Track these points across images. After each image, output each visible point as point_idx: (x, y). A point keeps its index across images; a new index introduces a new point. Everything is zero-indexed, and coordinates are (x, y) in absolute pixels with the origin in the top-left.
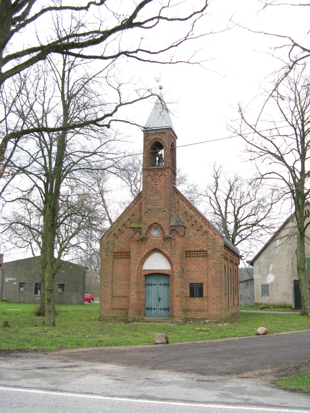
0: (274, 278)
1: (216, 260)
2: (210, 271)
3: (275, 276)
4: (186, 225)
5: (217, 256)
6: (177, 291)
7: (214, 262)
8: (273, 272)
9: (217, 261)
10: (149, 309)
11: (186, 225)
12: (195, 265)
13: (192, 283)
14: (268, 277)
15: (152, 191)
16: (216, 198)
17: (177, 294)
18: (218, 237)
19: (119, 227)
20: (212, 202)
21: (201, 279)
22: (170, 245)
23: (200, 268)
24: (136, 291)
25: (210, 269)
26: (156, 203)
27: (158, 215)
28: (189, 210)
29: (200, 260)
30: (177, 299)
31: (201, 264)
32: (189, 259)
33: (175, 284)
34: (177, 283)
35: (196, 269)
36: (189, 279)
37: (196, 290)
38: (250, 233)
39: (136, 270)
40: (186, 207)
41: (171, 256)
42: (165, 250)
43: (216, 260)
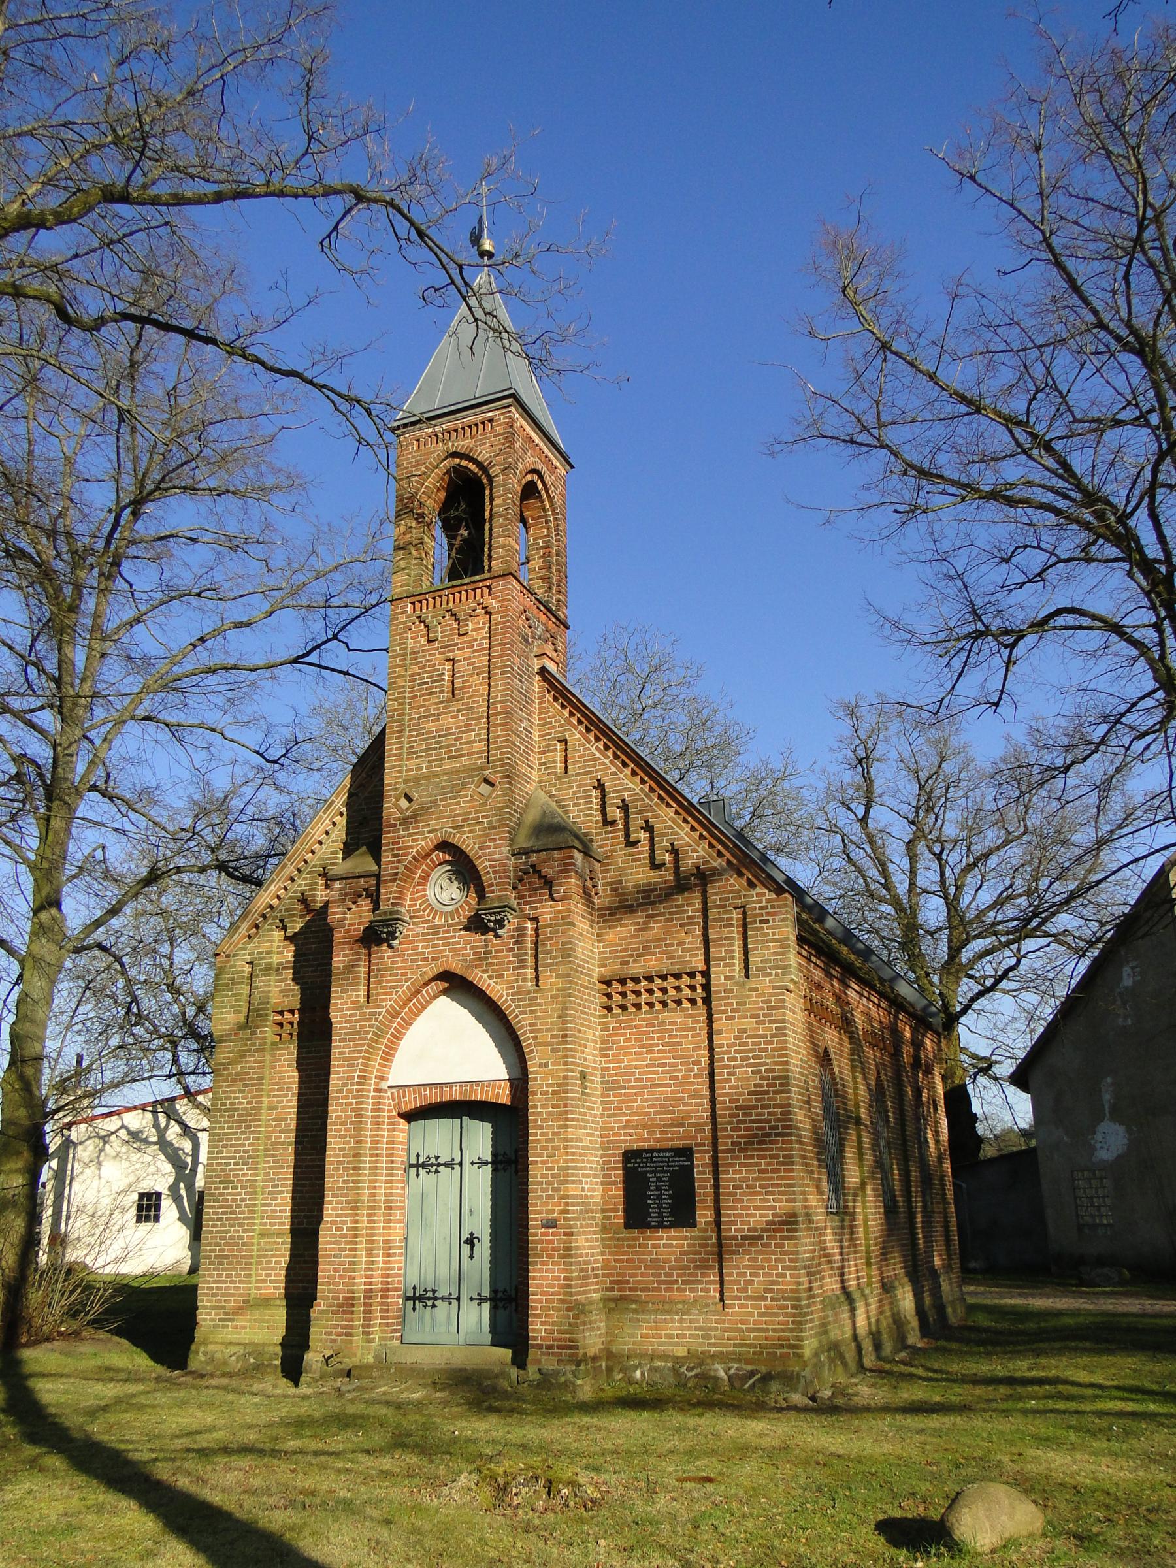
0: (1126, 1141)
1: (758, 1016)
2: (729, 1081)
3: (1129, 1131)
4: (601, 846)
5: (763, 995)
6: (548, 1197)
7: (745, 1030)
8: (1117, 1115)
9: (763, 1022)
10: (421, 1298)
11: (601, 846)
12: (649, 1052)
13: (635, 1146)
14: (1099, 1137)
15: (430, 694)
16: (871, 839)
17: (547, 1212)
18: (763, 895)
19: (299, 885)
20: (857, 854)
21: (682, 1125)
22: (512, 950)
23: (676, 1064)
24: (348, 1202)
25: (728, 1066)
26: (448, 746)
27: (459, 803)
28: (613, 773)
29: (675, 1023)
30: (548, 1242)
31: (679, 1044)
32: (620, 1022)
33: (541, 1155)
34: (546, 1148)
35: (657, 1072)
36: (624, 1128)
37: (658, 1188)
38: (1013, 961)
39: (351, 1091)
40: (599, 759)
41: (517, 1007)
42: (490, 977)
43: (758, 1016)
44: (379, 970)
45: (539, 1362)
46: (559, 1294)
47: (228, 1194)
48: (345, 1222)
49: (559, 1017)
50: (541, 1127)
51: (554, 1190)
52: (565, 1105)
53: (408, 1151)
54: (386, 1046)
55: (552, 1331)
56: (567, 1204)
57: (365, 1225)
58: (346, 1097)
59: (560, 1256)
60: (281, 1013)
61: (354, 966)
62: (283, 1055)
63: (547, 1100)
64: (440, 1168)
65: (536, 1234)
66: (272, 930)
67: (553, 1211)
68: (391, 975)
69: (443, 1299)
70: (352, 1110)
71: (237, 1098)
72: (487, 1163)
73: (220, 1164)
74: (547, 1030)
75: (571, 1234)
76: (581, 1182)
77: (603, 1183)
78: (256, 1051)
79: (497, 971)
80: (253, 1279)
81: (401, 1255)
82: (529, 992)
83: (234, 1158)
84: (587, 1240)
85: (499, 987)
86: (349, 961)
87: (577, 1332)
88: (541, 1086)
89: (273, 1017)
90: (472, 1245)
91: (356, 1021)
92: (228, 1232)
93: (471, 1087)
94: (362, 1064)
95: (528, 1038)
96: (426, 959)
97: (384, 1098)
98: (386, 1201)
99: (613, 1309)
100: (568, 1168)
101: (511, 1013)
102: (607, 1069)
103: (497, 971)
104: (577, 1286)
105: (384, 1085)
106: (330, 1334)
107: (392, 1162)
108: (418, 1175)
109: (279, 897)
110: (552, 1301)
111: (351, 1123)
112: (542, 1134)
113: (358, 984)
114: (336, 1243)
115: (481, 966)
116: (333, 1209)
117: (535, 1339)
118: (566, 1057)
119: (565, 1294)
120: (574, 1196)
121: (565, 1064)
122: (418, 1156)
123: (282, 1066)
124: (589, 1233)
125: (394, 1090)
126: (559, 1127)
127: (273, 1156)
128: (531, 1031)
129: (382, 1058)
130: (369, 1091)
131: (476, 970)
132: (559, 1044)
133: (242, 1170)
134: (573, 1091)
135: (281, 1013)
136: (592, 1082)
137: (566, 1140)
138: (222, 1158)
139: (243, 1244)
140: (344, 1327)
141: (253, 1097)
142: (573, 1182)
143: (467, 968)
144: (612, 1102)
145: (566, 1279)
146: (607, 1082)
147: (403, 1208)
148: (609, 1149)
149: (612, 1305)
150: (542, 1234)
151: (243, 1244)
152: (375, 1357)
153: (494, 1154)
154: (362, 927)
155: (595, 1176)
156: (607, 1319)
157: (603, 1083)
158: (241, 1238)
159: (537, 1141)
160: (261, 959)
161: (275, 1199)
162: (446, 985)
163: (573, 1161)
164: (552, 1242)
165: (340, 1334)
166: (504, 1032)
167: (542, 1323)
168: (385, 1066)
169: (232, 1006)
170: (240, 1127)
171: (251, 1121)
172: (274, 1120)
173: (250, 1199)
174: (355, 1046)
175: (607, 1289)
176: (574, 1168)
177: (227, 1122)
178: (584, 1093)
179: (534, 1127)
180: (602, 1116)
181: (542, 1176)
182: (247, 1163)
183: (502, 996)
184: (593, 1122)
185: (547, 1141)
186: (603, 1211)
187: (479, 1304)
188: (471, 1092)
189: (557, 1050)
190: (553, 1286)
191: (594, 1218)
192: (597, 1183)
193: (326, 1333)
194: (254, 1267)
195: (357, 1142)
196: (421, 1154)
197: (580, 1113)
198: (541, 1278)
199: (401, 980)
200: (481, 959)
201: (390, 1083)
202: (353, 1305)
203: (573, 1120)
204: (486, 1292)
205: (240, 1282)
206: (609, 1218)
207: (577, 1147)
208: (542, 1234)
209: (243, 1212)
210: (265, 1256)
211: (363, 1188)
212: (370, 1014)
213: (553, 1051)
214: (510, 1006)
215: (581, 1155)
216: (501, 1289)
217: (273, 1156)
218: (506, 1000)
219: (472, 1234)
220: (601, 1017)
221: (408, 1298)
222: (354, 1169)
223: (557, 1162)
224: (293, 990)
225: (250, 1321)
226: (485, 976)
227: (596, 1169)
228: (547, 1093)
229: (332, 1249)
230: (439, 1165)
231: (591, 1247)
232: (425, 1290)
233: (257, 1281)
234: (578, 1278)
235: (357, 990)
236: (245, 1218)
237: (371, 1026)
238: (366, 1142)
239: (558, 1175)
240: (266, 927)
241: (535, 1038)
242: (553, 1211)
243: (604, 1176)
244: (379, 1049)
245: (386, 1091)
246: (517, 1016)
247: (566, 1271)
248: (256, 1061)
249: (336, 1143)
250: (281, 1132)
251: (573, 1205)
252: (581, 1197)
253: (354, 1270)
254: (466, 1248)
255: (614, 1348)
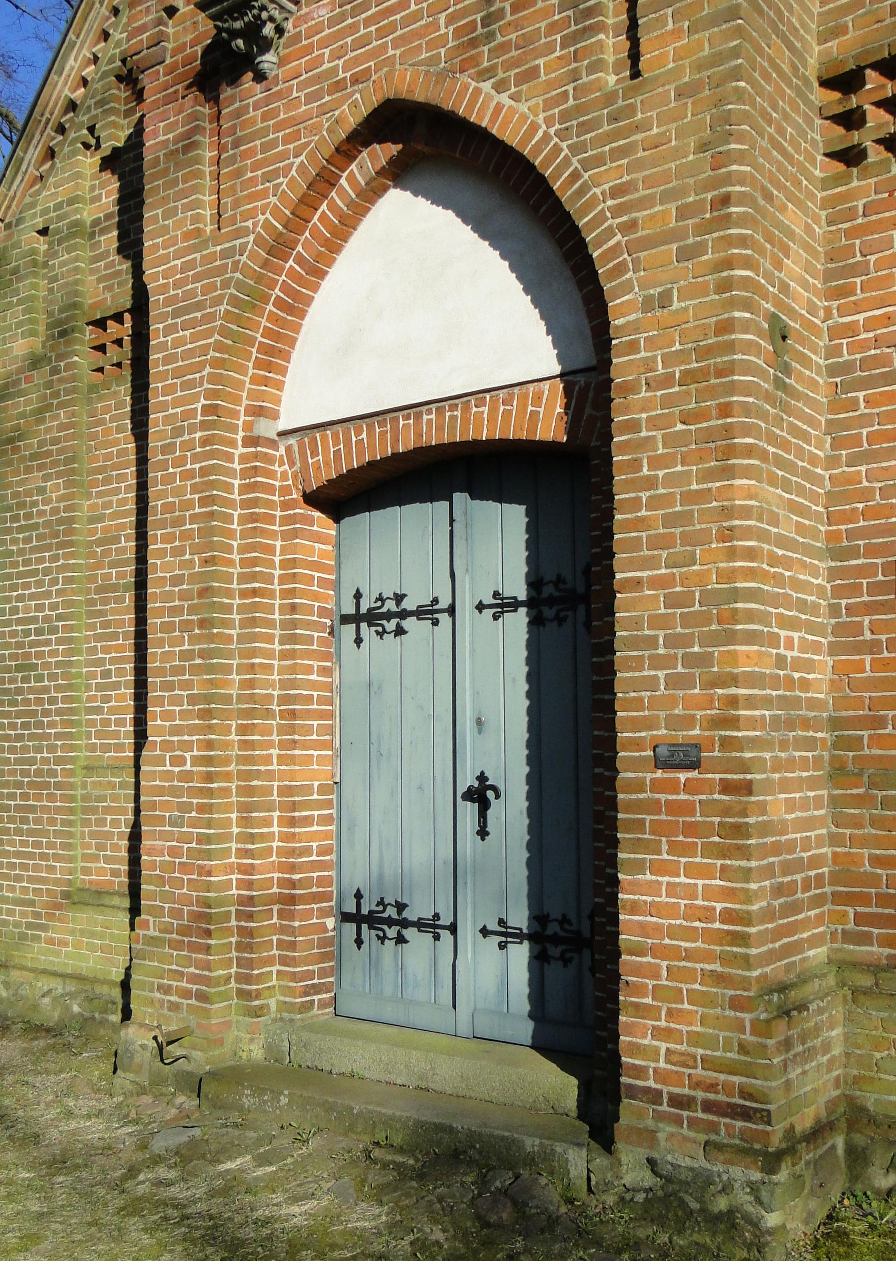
6: (673, 682)
10: (373, 920)
17: (673, 723)
19: (118, 44)
24: (192, 699)
30: (673, 808)
33: (649, 563)
41: (576, 149)
42: (500, 87)
44: (236, 144)
45: (649, 1137)
46: (708, 956)
47: (31, 690)
48: (187, 746)
49: (703, 147)
50: (651, 483)
51: (691, 660)
52: (725, 410)
53: (337, 586)
54: (267, 333)
55: (688, 1061)
56: (733, 702)
57: (236, 752)
58: (181, 461)
59: (710, 851)
60: (101, 324)
61: (187, 149)
62: (107, 409)
63: (666, 402)
64: (408, 623)
65: (639, 786)
66: (74, 153)
67: (690, 722)
68: (265, 148)
69: (420, 925)
70: (195, 489)
71: (35, 504)
72: (515, 604)
73: (14, 634)
74: (666, 197)
75: (747, 788)
76: (773, 641)
77: (833, 649)
78: (61, 405)
79: (516, 63)
80: (79, 852)
81: (325, 820)
82: (610, 98)
83: (35, 620)
84: (791, 806)
85: (523, 107)
86: (177, 140)
87: (767, 1072)
88: (649, 364)
89: (89, 334)
90: (484, 806)
91: (197, 278)
92: (33, 761)
93: (467, 408)
94: (212, 379)
95: (610, 233)
96: (339, 86)
97: (270, 460)
98: (284, 699)
99: (866, 992)
100: (736, 595)
101: (558, 173)
102: (850, 330)
103: (516, 63)
104: (763, 939)
105: (267, 429)
106: (167, 990)
107: (293, 608)
108: (359, 641)
109: (84, 82)
110: (688, 976)
111: (194, 518)
112: (654, 503)
113: (195, 190)
114: (175, 791)
115: (474, 61)
116: (168, 716)
117: (640, 1072)
118: (728, 263)
119: (724, 959)
120: (754, 680)
121: (725, 286)
122: (358, 596)
123: (107, 432)
124: (800, 785)
125: (292, 441)
126: (708, 476)
127: (101, 613)
128: (617, 211)
129: (258, 364)
130: (233, 444)
131: (464, 78)
132: (705, 228)
133: (48, 643)
134: (749, 368)
135: (101, 324)
136: (806, 361)
137: (727, 512)
138: (19, 622)
139: (58, 786)
140: (193, 979)
141: (60, 499)
142: (751, 638)
143: (441, 76)
144: (864, 421)
145: (728, 916)
146: (847, 368)
147: (330, 715)
148: (854, 552)
149: (865, 981)
150: (656, 786)
151: (58, 786)
152: (269, 1048)
153: (534, 583)
154: (199, 49)
155: (811, 628)
156: (849, 1019)
157: (833, 370)
158: (52, 773)
159: (640, 524)
160: (60, 218)
161: (107, 699)
162: (394, 149)
163: (750, 574)
164: (687, 808)
165: (186, 994)
166: (547, 250)
167: (658, 1033)
168: (266, 381)
169: (19, 325)
170: (41, 560)
171: (59, 546)
172: (100, 542)
173: (65, 699)
174: (194, 339)
175: (847, 936)
176: (752, 595)
177: (21, 552)
178: (780, 384)
179: (632, 485)
180: (832, 462)
181: (657, 622)
182: (53, 630)
183: (534, 127)
184: (807, 475)
185: (670, 520)
186: (835, 724)
187: (502, 946)
188: (466, 420)
189: (699, 249)
190: (690, 934)
191: (811, 744)
192: (816, 648)
193: (160, 988)
194: (77, 829)
195: (206, 562)
196: (365, 591)
197: (772, 439)
198: (654, 909)
199: (283, 156)
200: (474, 43)
201: (283, 424)
202: (208, 933)
203: (749, 451)
204: (520, 918)
205: (57, 858)
206: (854, 744)
207: (763, 536)
208: (656, 786)
209: (52, 725)
210: (94, 810)
211: (228, 669)
212: (224, 254)
213: (685, 254)
214: (557, 150)
215: (774, 560)
216: (555, 913)
217: (101, 613)
218: (546, 137)
219: (482, 778)
220: (825, 184)
221: (346, 917)
222: (202, 624)
223: (702, 577)
224: (118, 273)
225: (72, 932)
226: (487, 86)
227: (814, 609)
228: (667, 380)
229: (165, 805)
230: (404, 614)
231: (808, 824)
232: (381, 902)
233: (86, 858)
234: (768, 914)
235: (198, 204)
236: (58, 736)
237: (225, 285)
238: (230, 563)
239: (704, 619)
240: (66, 150)
241: (631, 226)
242: (689, 722)
243: (838, 630)
244: (251, 341)
245: (272, 444)
246: (576, 176)
247: (728, 894)
248: (61, 428)
249: (167, 567)
250: (112, 565)
251: (751, 702)
252: (775, 682)
253: (209, 855)
254: (469, 810)
255: (870, 1099)
